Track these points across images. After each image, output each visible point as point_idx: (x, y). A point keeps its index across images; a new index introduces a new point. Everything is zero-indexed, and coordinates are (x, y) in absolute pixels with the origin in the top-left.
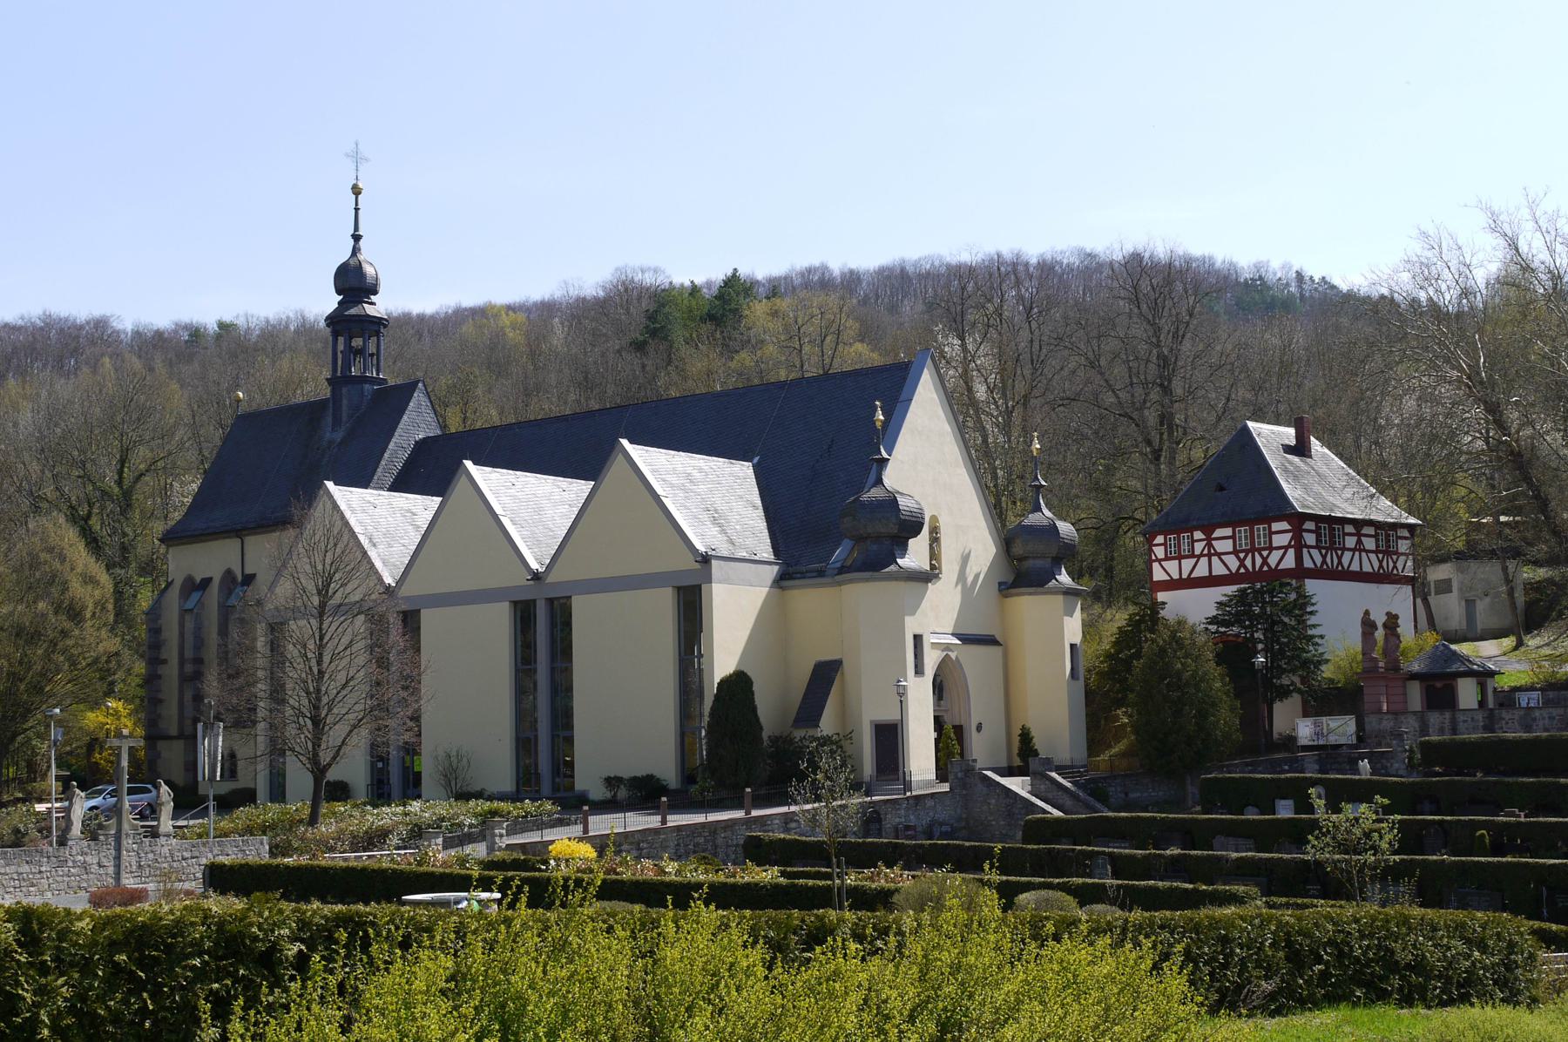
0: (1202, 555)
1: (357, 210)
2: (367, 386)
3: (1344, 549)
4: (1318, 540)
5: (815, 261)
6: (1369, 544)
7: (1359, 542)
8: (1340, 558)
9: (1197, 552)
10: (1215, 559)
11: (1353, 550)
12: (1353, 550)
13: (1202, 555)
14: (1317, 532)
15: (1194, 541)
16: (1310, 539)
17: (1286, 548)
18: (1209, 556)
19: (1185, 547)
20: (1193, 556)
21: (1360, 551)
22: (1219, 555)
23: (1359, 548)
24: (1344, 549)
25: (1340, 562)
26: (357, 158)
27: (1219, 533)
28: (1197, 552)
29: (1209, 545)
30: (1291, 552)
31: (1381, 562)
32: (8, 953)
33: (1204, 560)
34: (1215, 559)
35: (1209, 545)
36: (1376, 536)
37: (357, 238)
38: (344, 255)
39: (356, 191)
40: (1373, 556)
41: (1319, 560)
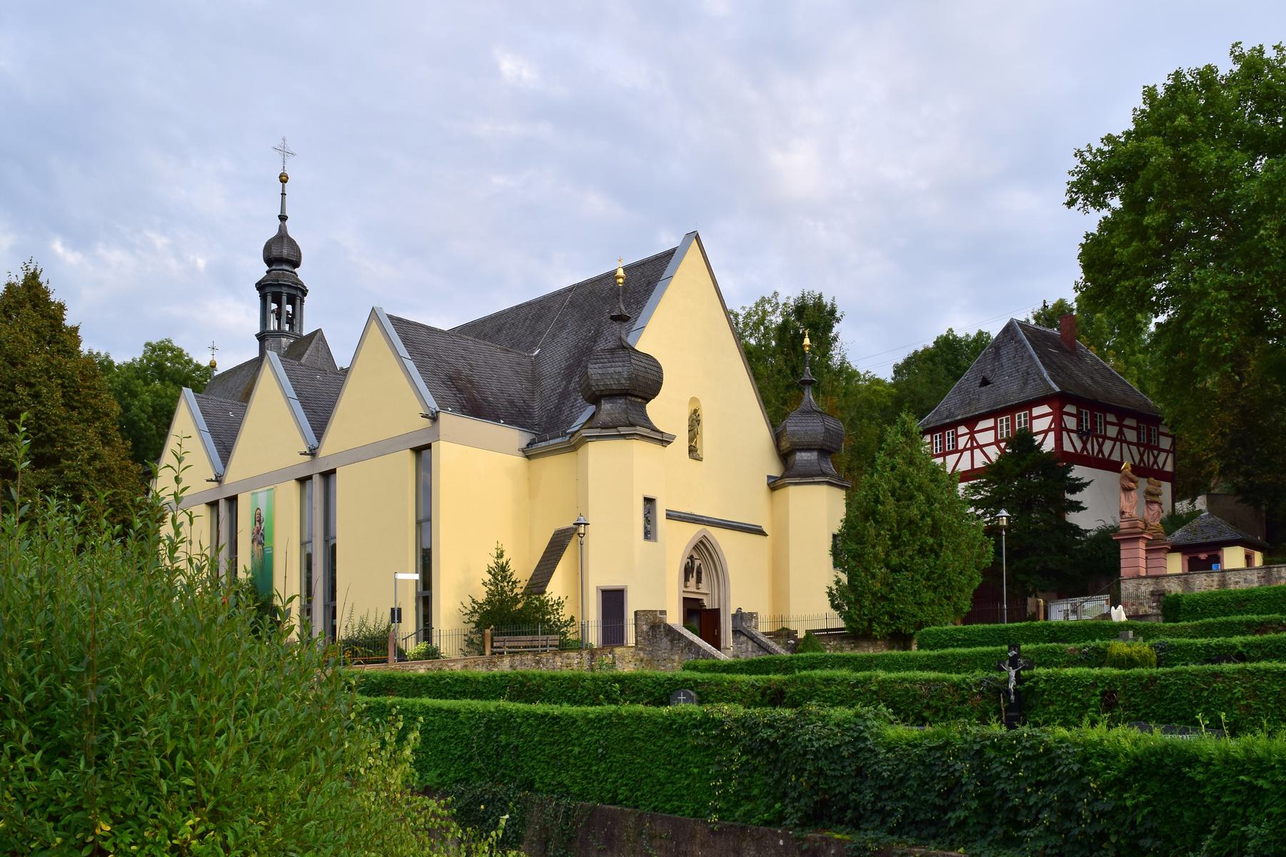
0: (965, 449)
1: (283, 194)
2: (284, 340)
3: (1105, 437)
4: (1079, 423)
5: (827, 544)
6: (1131, 435)
7: (1121, 432)
8: (1101, 446)
9: (961, 447)
10: (977, 451)
11: (1115, 440)
12: (1115, 440)
13: (965, 449)
14: (1078, 416)
15: (958, 436)
16: (1071, 423)
17: (1046, 432)
18: (972, 449)
19: (949, 446)
20: (956, 451)
21: (1122, 442)
22: (980, 447)
23: (1120, 438)
24: (1105, 437)
25: (1100, 451)
26: (285, 152)
27: (982, 425)
28: (961, 447)
29: (972, 439)
30: (1051, 435)
31: (1142, 455)
32: (1210, 851)
33: (967, 454)
34: (977, 451)
35: (972, 439)
36: (1137, 429)
37: (283, 218)
38: (273, 232)
39: (284, 179)
40: (1134, 448)
41: (1079, 446)
